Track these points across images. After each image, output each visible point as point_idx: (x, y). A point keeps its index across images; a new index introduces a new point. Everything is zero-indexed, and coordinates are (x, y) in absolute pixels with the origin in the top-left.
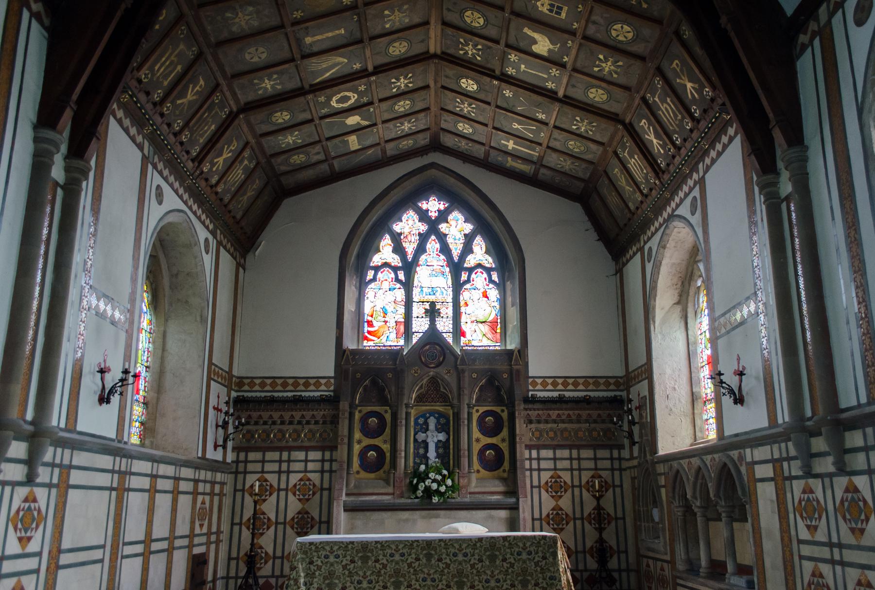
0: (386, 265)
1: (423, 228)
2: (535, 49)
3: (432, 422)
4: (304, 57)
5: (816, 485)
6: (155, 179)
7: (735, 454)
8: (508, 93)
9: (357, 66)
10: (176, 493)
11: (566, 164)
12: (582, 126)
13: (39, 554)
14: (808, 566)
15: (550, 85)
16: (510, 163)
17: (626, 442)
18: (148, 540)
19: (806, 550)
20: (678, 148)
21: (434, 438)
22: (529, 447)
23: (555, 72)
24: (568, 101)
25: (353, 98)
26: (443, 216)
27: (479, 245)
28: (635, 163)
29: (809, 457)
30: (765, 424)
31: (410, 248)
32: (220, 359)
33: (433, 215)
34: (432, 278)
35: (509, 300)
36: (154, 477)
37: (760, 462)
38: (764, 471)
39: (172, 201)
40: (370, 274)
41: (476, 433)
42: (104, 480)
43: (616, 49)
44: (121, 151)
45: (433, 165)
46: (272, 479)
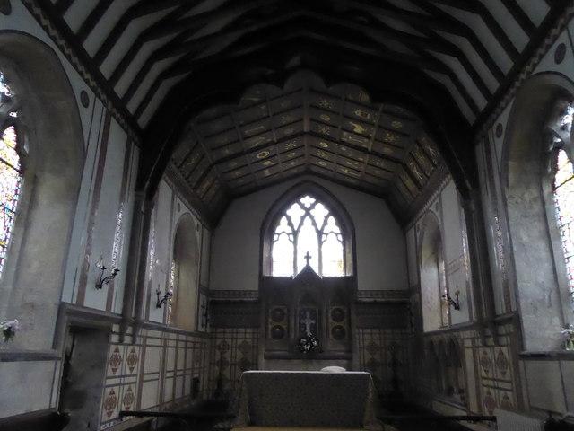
1: (303, 212)
2: (355, 130)
3: (308, 314)
4: (245, 139)
5: (488, 350)
6: (178, 201)
7: (455, 334)
8: (343, 149)
9: (269, 140)
10: (186, 348)
11: (375, 181)
12: (382, 164)
13: (136, 375)
14: (485, 389)
15: (364, 146)
16: (347, 180)
17: (409, 325)
18: (176, 370)
19: (508, 386)
20: (428, 177)
21: (309, 323)
22: (358, 327)
23: (366, 140)
24: (373, 153)
25: (267, 153)
26: (313, 206)
27: (332, 220)
28: (409, 182)
29: (485, 337)
30: (468, 320)
32: (204, 283)
34: (308, 236)
35: (347, 250)
36: (177, 341)
37: (467, 338)
38: (468, 343)
39: (184, 209)
40: (276, 237)
41: (331, 320)
42: (158, 342)
43: (393, 131)
44: (165, 191)
45: (307, 181)
46: (229, 341)
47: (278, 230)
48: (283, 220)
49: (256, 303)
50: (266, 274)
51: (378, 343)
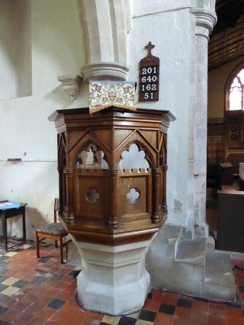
40: (231, 90)
47: (233, 85)
48: (236, 80)
49: (224, 123)
50: (227, 109)
51: (220, 142)
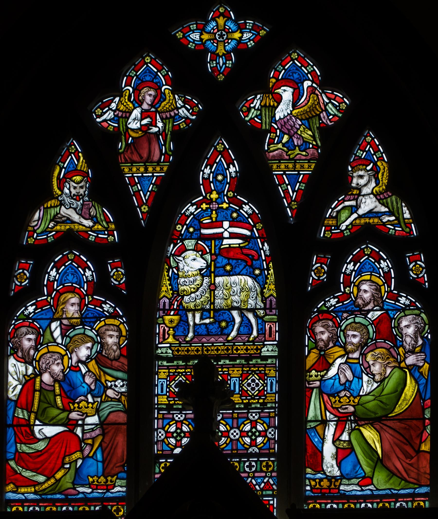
0: (72, 240)
26: (253, 72)
31: (143, 180)
33: (221, 66)
34: (211, 280)
